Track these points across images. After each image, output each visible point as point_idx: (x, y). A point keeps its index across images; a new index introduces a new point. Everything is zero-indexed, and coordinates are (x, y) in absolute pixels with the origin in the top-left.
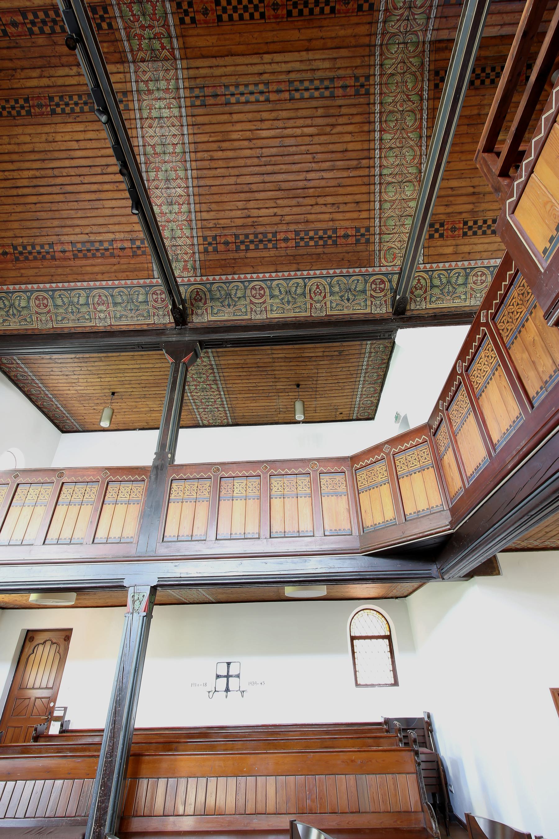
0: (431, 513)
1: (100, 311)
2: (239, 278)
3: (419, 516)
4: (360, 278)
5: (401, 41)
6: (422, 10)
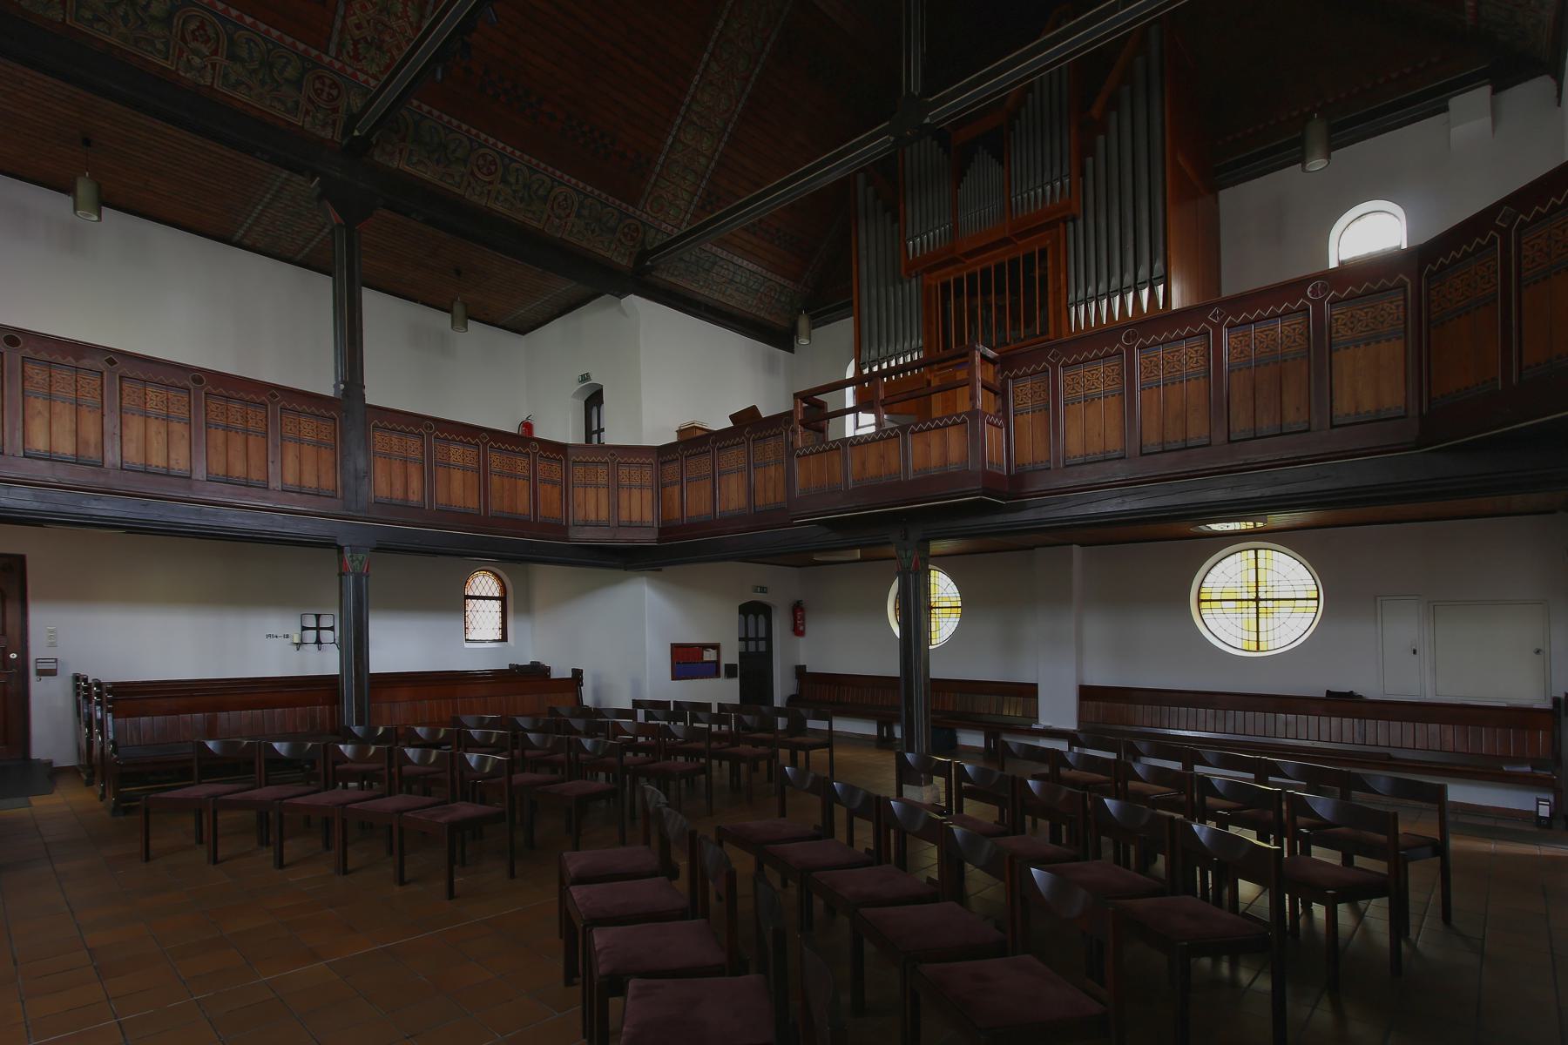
0: (641, 526)
1: (196, 52)
2: (468, 131)
3: (630, 525)
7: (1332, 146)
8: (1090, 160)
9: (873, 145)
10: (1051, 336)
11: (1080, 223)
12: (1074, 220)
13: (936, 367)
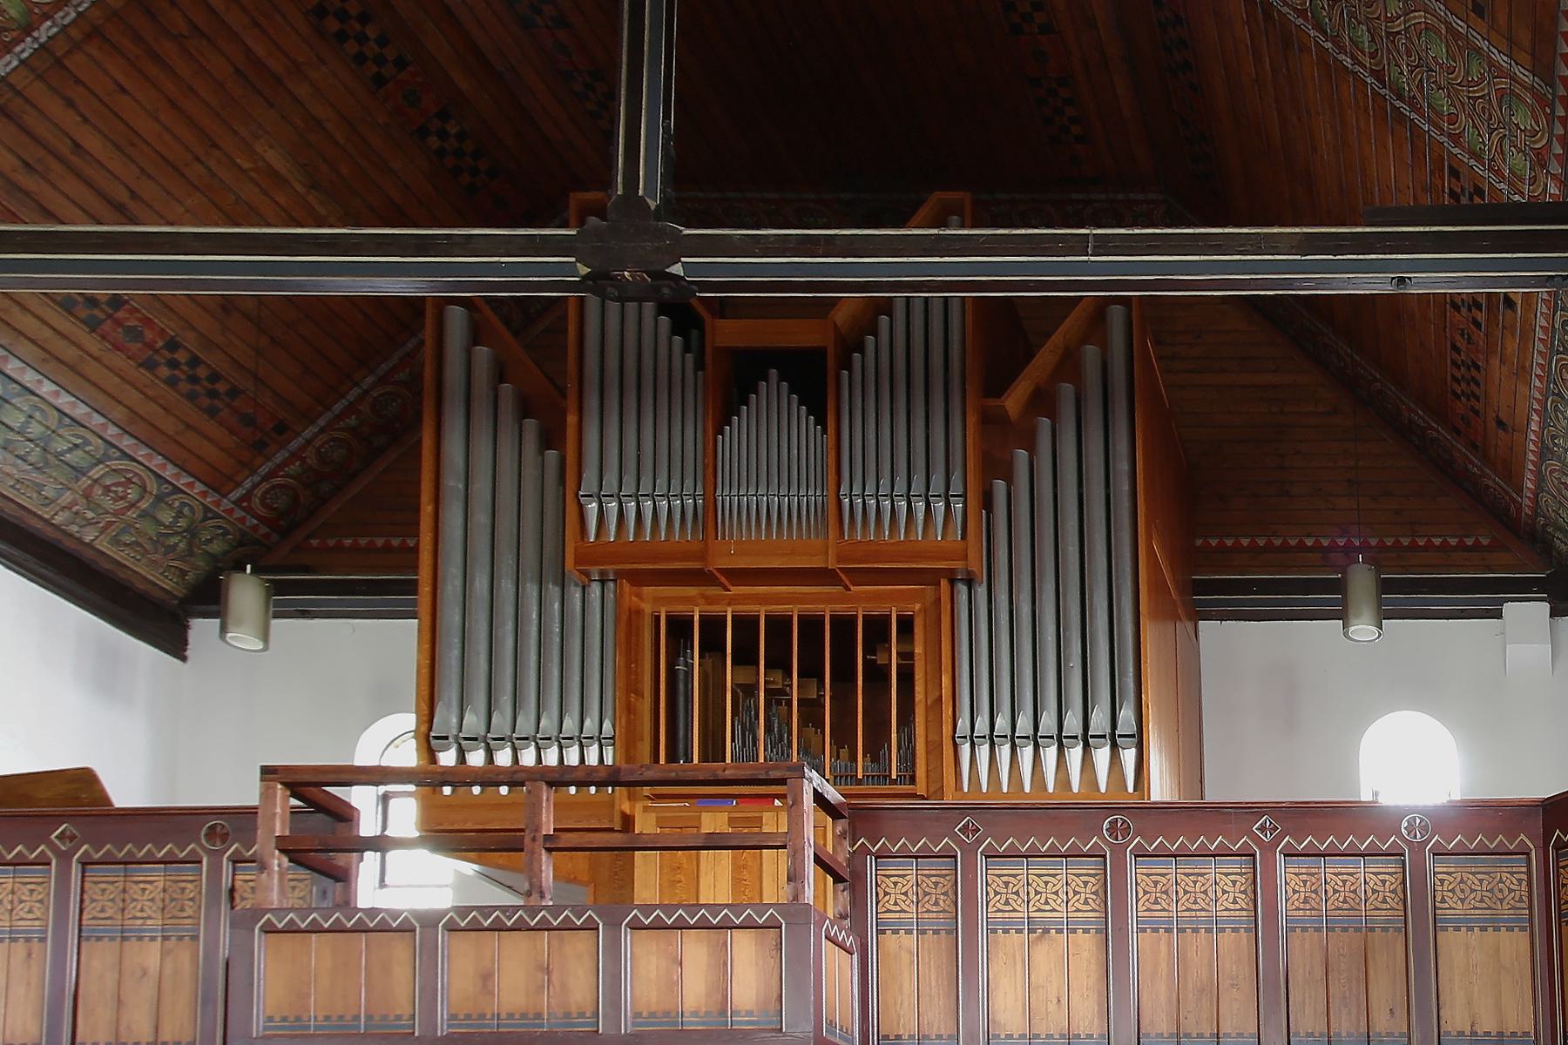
7: (1384, 614)
8: (1000, 485)
9: (525, 261)
10: (920, 788)
11: (981, 591)
12: (970, 583)
13: (646, 790)
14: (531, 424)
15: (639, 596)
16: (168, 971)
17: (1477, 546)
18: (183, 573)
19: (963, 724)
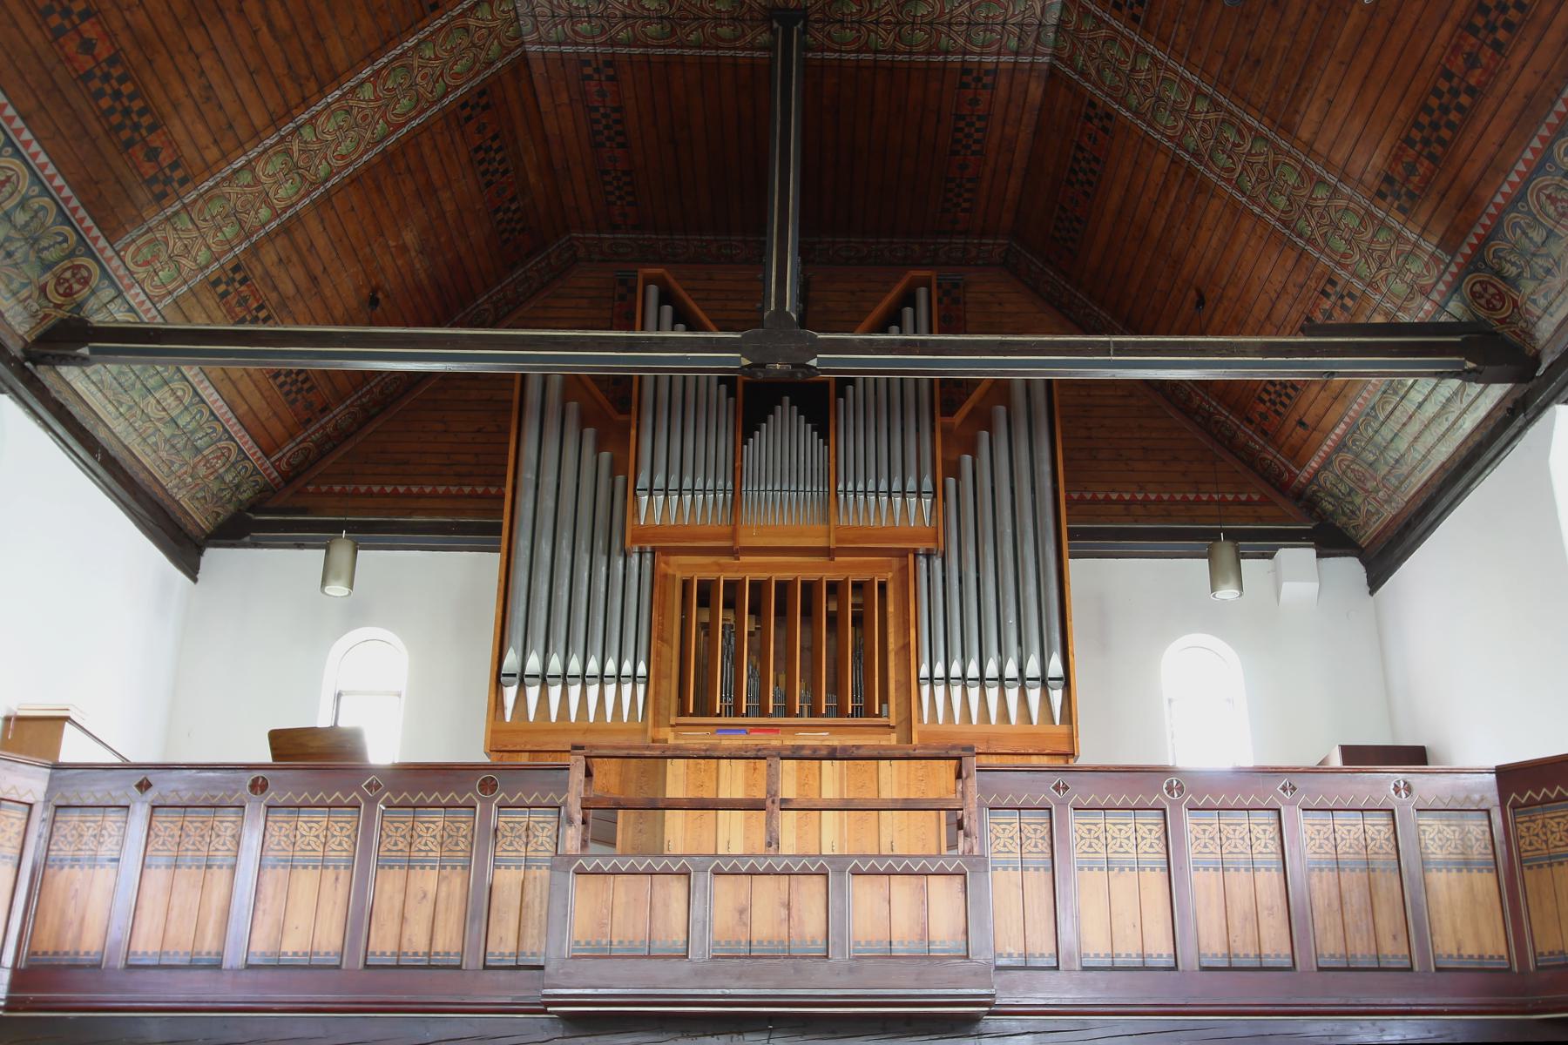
4: (73, 238)
5: (520, 11)
6: (570, 33)
8: (951, 481)
14: (589, 433)
15: (667, 563)
16: (443, 894)
17: (1249, 502)
18: (218, 514)
19: (924, 672)
